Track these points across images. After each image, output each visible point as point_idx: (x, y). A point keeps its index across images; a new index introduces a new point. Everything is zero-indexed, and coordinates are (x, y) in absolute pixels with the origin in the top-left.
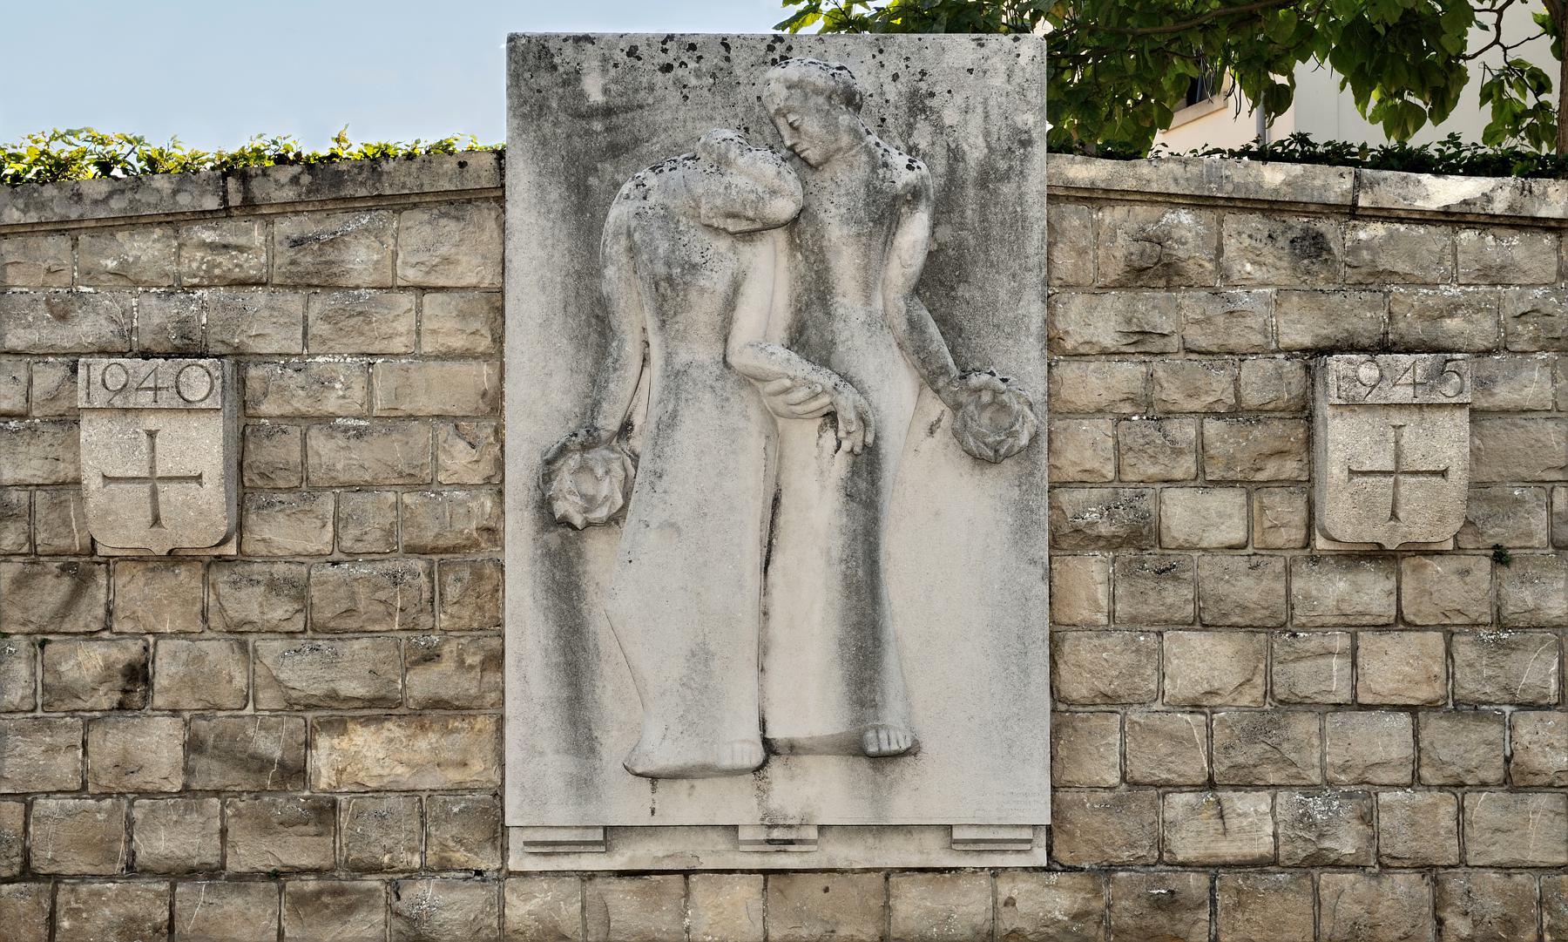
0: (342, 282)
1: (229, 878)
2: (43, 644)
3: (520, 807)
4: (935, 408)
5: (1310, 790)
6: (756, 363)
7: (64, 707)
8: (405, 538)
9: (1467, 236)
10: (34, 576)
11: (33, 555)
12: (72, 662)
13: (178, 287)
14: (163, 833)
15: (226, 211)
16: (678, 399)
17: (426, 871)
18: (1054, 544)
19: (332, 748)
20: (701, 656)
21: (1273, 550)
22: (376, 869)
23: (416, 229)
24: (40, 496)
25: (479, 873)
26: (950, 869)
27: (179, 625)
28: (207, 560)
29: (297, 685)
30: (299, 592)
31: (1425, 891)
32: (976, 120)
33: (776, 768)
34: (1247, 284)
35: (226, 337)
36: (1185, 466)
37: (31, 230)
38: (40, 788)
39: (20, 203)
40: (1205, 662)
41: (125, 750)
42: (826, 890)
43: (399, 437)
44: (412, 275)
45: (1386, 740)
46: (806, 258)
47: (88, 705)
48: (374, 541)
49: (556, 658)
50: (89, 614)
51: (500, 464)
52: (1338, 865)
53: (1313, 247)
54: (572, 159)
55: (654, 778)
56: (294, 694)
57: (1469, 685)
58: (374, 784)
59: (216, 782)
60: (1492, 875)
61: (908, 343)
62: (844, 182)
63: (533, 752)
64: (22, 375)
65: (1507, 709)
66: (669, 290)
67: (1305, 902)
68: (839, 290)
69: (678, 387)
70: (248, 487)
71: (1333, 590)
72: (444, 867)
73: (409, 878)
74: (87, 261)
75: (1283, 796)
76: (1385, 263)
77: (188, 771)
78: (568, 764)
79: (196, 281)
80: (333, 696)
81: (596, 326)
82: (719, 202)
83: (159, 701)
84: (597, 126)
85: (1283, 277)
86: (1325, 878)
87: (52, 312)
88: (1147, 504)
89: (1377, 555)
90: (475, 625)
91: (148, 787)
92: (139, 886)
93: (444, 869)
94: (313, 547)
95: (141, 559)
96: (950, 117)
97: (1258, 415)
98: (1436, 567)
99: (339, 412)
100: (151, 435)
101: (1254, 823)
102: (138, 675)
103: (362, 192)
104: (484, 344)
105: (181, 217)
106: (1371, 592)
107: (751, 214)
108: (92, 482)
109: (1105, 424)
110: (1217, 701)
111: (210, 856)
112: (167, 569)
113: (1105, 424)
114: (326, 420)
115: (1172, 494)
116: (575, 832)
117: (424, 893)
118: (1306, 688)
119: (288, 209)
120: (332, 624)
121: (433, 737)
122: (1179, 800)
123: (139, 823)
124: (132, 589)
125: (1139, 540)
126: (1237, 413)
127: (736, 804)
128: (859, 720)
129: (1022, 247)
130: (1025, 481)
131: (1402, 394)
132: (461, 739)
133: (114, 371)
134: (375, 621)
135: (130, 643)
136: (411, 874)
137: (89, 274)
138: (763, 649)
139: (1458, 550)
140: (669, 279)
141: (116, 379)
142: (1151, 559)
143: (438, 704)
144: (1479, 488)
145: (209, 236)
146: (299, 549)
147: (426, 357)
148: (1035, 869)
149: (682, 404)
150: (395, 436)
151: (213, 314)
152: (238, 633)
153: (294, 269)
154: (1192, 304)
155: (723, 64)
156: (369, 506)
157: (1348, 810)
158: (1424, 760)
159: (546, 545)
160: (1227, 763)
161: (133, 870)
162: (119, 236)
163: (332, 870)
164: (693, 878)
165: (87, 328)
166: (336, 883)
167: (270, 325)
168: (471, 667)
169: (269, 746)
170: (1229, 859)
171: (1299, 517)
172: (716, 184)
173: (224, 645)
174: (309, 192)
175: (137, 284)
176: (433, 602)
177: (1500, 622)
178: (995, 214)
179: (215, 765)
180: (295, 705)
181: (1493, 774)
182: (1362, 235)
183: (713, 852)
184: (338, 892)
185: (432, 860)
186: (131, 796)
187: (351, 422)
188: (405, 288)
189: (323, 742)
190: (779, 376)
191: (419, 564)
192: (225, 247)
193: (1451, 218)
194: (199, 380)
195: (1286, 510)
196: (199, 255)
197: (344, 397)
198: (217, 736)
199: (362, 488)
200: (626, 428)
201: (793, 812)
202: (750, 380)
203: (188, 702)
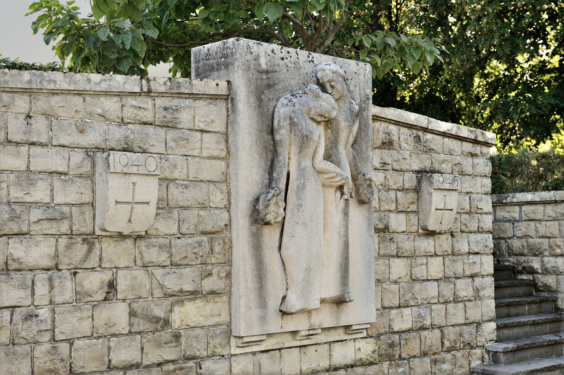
0: (178, 126)
1: (144, 368)
2: (75, 274)
3: (245, 329)
6: (326, 167)
7: (85, 301)
8: (201, 228)
10: (73, 244)
12: (88, 281)
14: (123, 351)
16: (304, 179)
19: (180, 311)
24: (74, 209)
25: (223, 356)
26: (344, 340)
27: (127, 264)
28: (134, 237)
29: (170, 287)
32: (357, 90)
35: (142, 145)
36: (393, 207)
37: (69, 92)
38: (77, 336)
39: (67, 80)
41: (109, 317)
42: (316, 351)
43: (198, 188)
44: (202, 126)
46: (332, 132)
47: (93, 299)
49: (255, 273)
50: (93, 261)
54: (257, 88)
56: (169, 291)
58: (192, 325)
59: (141, 328)
60: (451, 328)
61: (352, 163)
63: (249, 308)
64: (67, 157)
65: (454, 279)
68: (340, 144)
69: (304, 174)
73: (202, 360)
74: (89, 109)
75: (414, 308)
77: (131, 325)
79: (130, 121)
80: (181, 291)
82: (318, 110)
83: (120, 296)
84: (264, 77)
86: (424, 333)
87: (77, 129)
90: (223, 262)
91: (117, 332)
93: (213, 356)
94: (172, 232)
99: (178, 178)
100: (134, 184)
102: (112, 286)
103: (187, 91)
104: (224, 154)
105: (124, 94)
107: (327, 115)
110: (401, 280)
112: (122, 240)
116: (259, 337)
119: (161, 95)
120: (179, 263)
121: (211, 305)
123: (113, 348)
124: (112, 251)
126: (403, 190)
128: (343, 290)
129: (368, 133)
131: (447, 186)
132: (219, 305)
134: (192, 261)
135: (108, 272)
140: (307, 136)
145: (134, 103)
146: (167, 233)
147: (204, 158)
148: (364, 338)
149: (306, 180)
150: (197, 188)
151: (136, 135)
153: (165, 119)
155: (297, 60)
156: (190, 216)
158: (440, 295)
159: (252, 231)
160: (404, 300)
162: (101, 98)
163: (178, 360)
164: (282, 351)
165: (92, 138)
166: (179, 365)
168: (222, 277)
169: (159, 312)
170: (404, 330)
173: (143, 272)
174: (170, 89)
175: (107, 120)
179: (141, 321)
180: (167, 296)
181: (452, 299)
182: (428, 137)
184: (181, 369)
185: (210, 353)
186: (109, 337)
187: (181, 182)
188: (197, 130)
190: (333, 172)
191: (205, 238)
192: (140, 108)
193: (444, 135)
196: (131, 110)
197: (181, 172)
198: (142, 309)
199: (185, 208)
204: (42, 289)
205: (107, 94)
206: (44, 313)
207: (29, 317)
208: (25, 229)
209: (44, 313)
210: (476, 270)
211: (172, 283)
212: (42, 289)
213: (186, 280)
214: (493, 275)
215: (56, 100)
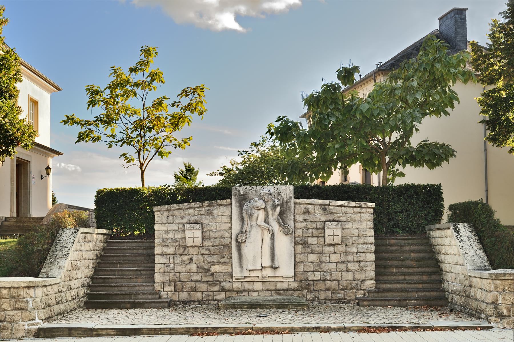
4: (281, 229)
5: (325, 272)
9: (343, 208)
11: (180, 246)
13: (195, 215)
15: (200, 207)
17: (224, 281)
18: (295, 244)
20: (254, 257)
22: (218, 281)
23: (438, 231)
30: (209, 250)
31: (337, 283)
32: (285, 196)
33: (263, 270)
34: (317, 214)
36: (310, 235)
37: (179, 209)
40: (313, 257)
44: (221, 214)
48: (217, 244)
50: (186, 253)
51: (231, 235)
52: (328, 280)
53: (325, 209)
54: (239, 200)
55: (249, 271)
57: (343, 260)
62: (270, 204)
63: (236, 268)
66: (250, 216)
67: (324, 285)
70: (203, 238)
71: (327, 249)
72: (226, 281)
76: (333, 211)
78: (240, 269)
80: (213, 262)
81: (242, 220)
85: (322, 213)
86: (326, 282)
88: (306, 239)
95: (192, 246)
96: (282, 195)
97: (319, 229)
98: (339, 246)
101: (318, 276)
102: (191, 259)
104: (229, 221)
106: (332, 249)
108: (187, 238)
109: (301, 230)
111: (200, 279)
113: (301, 230)
114: (211, 230)
115: (309, 238)
117: (224, 284)
122: (309, 273)
124: (191, 250)
125: (305, 244)
126: (316, 229)
127: (259, 274)
130: (291, 237)
131: (334, 227)
132: (228, 267)
133: (189, 225)
136: (222, 282)
137: (185, 214)
138: (262, 256)
141: (189, 226)
142: (306, 246)
143: (225, 263)
152: (202, 255)
154: (311, 216)
161: (192, 281)
165: (185, 220)
167: (205, 219)
169: (206, 267)
172: (256, 204)
176: (224, 251)
177: (346, 252)
178: (288, 206)
180: (209, 263)
183: (256, 279)
189: (212, 267)
193: (341, 206)
194: (198, 226)
195: (322, 240)
199: (216, 238)
200: (246, 231)
202: (260, 226)
203: (197, 262)
204: (171, 259)
205: (190, 208)
206: (172, 265)
207: (168, 266)
208: (167, 244)
209: (172, 265)
210: (362, 259)
211: (210, 259)
212: (171, 259)
213: (215, 259)
214: (374, 262)
215: (175, 212)
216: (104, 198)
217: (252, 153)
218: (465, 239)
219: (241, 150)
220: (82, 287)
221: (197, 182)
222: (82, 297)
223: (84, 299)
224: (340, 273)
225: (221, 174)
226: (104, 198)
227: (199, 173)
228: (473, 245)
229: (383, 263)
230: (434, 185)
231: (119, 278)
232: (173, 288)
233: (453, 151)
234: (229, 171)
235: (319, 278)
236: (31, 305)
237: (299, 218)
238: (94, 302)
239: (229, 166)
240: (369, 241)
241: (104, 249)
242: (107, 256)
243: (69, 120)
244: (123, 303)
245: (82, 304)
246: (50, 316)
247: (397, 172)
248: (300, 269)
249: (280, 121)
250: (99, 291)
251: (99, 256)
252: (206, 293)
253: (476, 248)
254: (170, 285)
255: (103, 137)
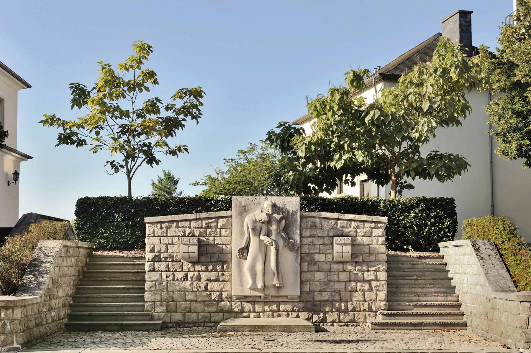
5: (332, 292)
21: (328, 262)
36: (317, 251)
40: (319, 276)
45: (342, 286)
71: (335, 267)
89: (340, 262)
92: (187, 303)
97: (327, 245)
101: (325, 296)
106: (340, 267)
109: (308, 246)
113: (308, 246)
115: (316, 255)
118: (332, 279)
131: (343, 242)
139: (351, 262)
144: (352, 254)
157: (337, 294)
171: (331, 257)
178: (293, 219)
201: (268, 294)
216: (85, 206)
217: (240, 161)
218: (486, 257)
219: (227, 158)
220: (63, 307)
221: (178, 191)
222: (63, 318)
223: (66, 321)
224: (349, 293)
225: (206, 184)
226: (85, 206)
227: (178, 183)
228: (495, 264)
229: (394, 281)
230: (447, 199)
231: (105, 297)
232: (164, 308)
233: (466, 164)
234: (214, 180)
235: (327, 299)
236: (9, 327)
237: (307, 233)
238: (77, 325)
239: (214, 175)
240: (381, 259)
241: (86, 264)
242: (90, 272)
243: (51, 121)
244: (109, 325)
245: (63, 326)
246: (30, 339)
247: (405, 184)
248: (306, 289)
249: (282, 128)
250: (81, 312)
251: (81, 272)
252: (202, 314)
253: (498, 267)
254: (161, 305)
255: (88, 141)
